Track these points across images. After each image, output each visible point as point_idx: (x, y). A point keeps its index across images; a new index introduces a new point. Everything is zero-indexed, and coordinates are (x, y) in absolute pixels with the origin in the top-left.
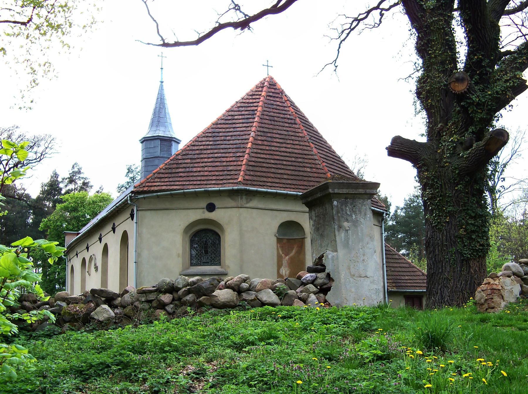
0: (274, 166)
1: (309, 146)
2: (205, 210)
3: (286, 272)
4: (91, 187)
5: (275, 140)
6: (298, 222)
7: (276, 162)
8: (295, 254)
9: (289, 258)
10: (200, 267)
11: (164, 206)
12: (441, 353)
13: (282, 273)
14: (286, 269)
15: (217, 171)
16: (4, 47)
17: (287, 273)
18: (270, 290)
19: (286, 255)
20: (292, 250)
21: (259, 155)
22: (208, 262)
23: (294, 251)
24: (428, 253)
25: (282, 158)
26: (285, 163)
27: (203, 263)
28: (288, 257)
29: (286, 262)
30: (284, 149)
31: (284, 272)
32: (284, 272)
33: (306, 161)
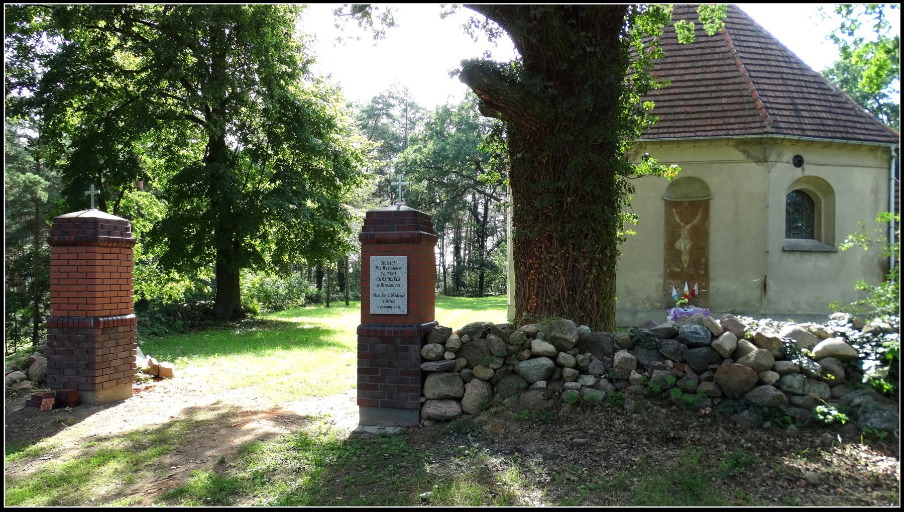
1: (735, 64)
3: (685, 245)
4: (453, 74)
5: (678, 66)
6: (700, 177)
7: (672, 97)
8: (700, 221)
9: (691, 227)
13: (680, 247)
14: (686, 242)
16: (191, 404)
18: (426, 347)
19: (687, 223)
20: (696, 215)
23: (698, 217)
25: (682, 90)
28: (689, 225)
29: (686, 232)
30: (690, 77)
31: (682, 246)
32: (682, 246)
33: (724, 88)
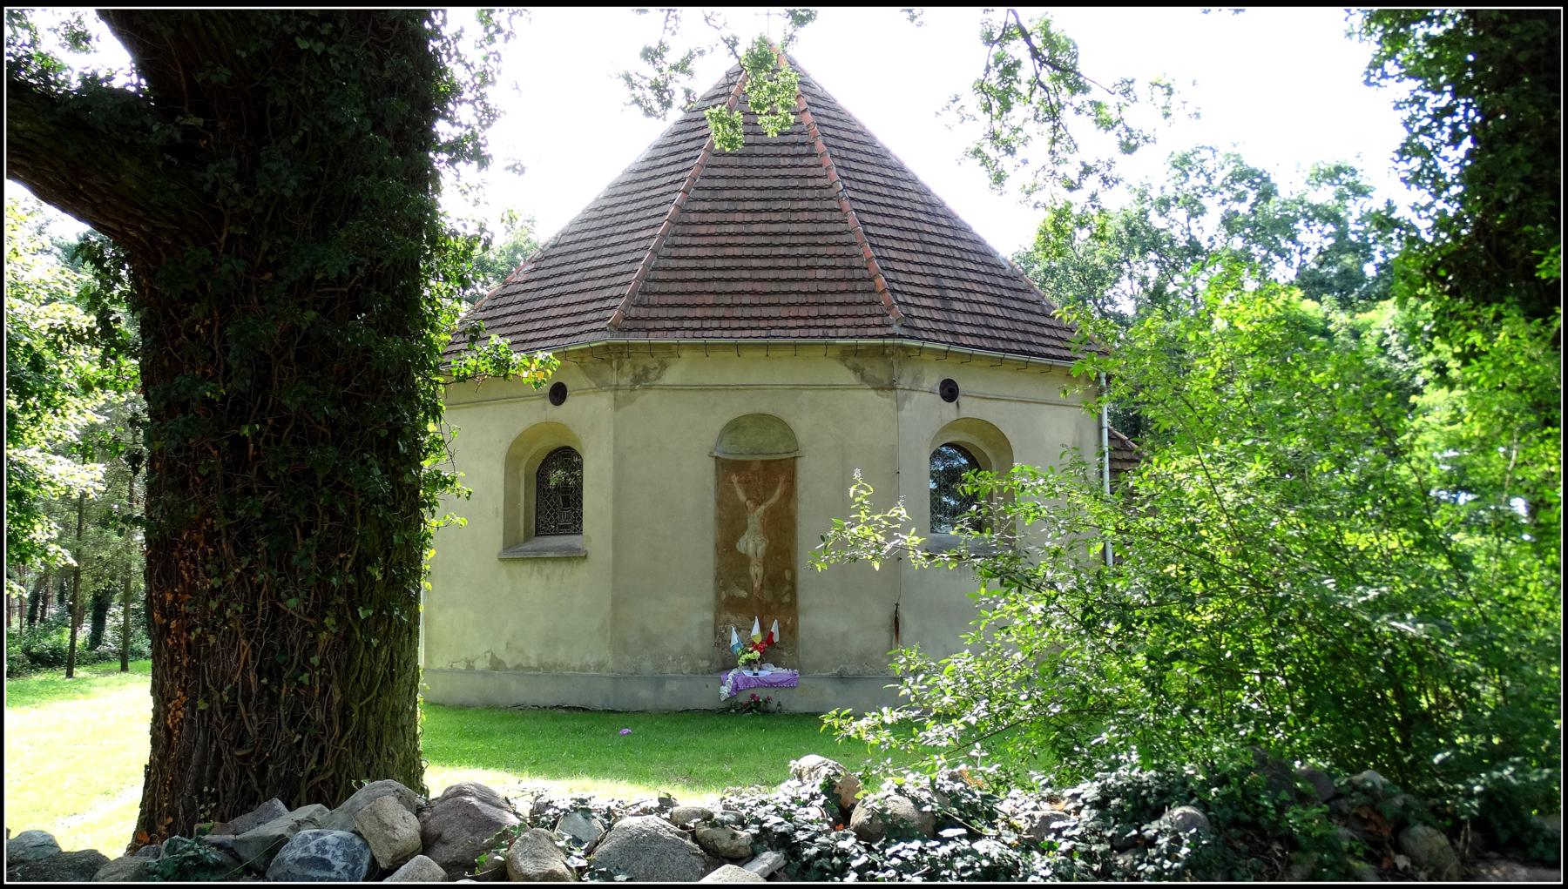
0: (717, 274)
1: (840, 210)
2: (548, 401)
6: (779, 414)
8: (781, 499)
10: (562, 538)
11: (1040, 396)
12: (1420, 647)
14: (758, 539)
15: (580, 303)
17: (760, 549)
19: (758, 503)
20: (775, 488)
21: (683, 252)
22: (567, 527)
23: (778, 492)
24: (158, 635)
26: (755, 263)
27: (561, 527)
28: (763, 507)
29: (757, 520)
31: (751, 545)
32: (751, 545)
